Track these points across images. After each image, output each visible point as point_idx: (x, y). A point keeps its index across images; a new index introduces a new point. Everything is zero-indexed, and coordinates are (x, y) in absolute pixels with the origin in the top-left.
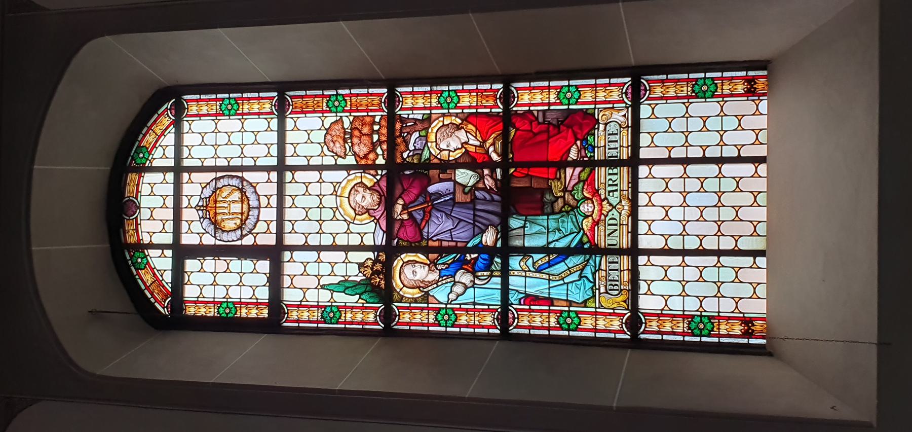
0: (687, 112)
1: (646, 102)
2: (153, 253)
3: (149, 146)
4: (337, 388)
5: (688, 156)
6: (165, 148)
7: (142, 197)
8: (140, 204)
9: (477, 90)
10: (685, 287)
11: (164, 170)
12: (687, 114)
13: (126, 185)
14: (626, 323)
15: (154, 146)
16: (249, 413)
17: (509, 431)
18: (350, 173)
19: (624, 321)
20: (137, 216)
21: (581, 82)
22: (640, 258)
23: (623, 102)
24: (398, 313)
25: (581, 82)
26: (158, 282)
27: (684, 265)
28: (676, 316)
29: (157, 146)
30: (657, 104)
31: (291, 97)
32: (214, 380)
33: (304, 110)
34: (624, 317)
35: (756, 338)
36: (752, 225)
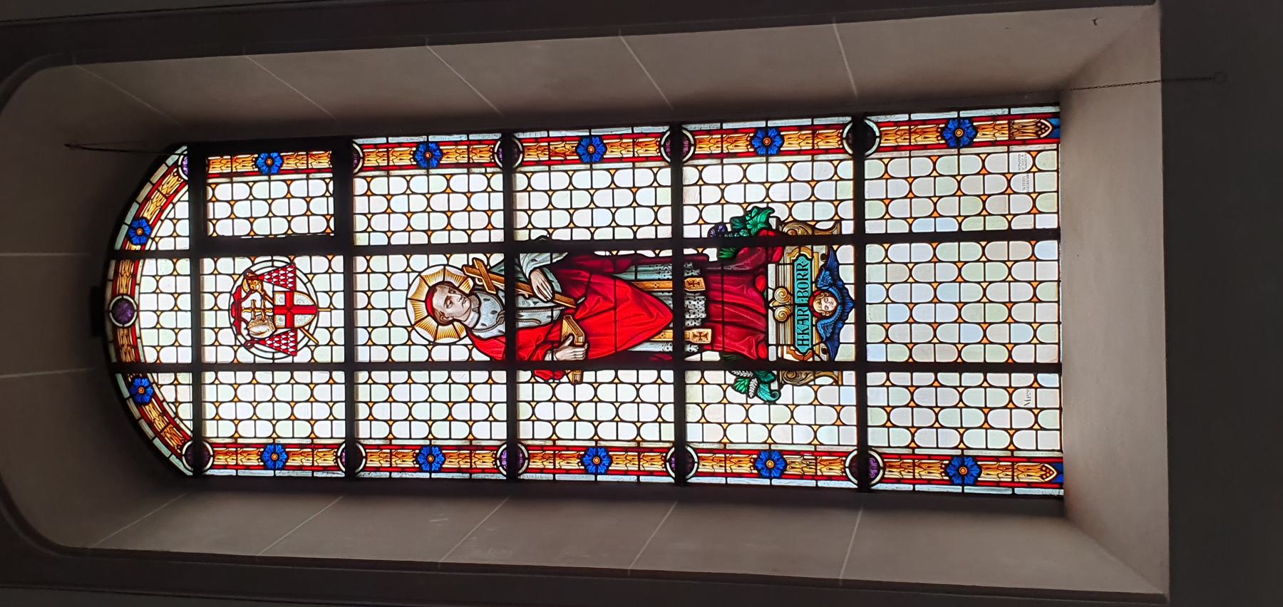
0: (935, 169)
1: (691, 162)
2: (165, 378)
3: (151, 218)
4: (259, 555)
5: (937, 230)
6: (175, 221)
7: (141, 295)
8: (138, 306)
9: (721, 131)
10: (453, 409)
11: (174, 255)
12: (836, 176)
13: (118, 276)
14: (850, 467)
15: (158, 218)
16: (302, 600)
17: (416, 605)
18: (256, 262)
19: (847, 464)
20: (134, 323)
21: (803, 122)
22: (504, 373)
23: (842, 151)
24: (364, 454)
25: (977, 113)
26: (172, 421)
27: (936, 385)
28: (654, 450)
29: (163, 217)
30: (989, 154)
31: (693, 133)
32: (444, 558)
33: (568, 158)
34: (847, 458)
35: (887, 483)
36: (1031, 328)
